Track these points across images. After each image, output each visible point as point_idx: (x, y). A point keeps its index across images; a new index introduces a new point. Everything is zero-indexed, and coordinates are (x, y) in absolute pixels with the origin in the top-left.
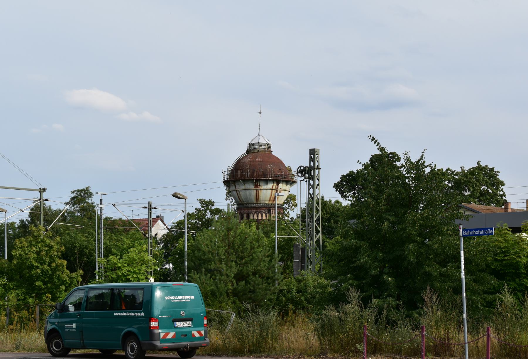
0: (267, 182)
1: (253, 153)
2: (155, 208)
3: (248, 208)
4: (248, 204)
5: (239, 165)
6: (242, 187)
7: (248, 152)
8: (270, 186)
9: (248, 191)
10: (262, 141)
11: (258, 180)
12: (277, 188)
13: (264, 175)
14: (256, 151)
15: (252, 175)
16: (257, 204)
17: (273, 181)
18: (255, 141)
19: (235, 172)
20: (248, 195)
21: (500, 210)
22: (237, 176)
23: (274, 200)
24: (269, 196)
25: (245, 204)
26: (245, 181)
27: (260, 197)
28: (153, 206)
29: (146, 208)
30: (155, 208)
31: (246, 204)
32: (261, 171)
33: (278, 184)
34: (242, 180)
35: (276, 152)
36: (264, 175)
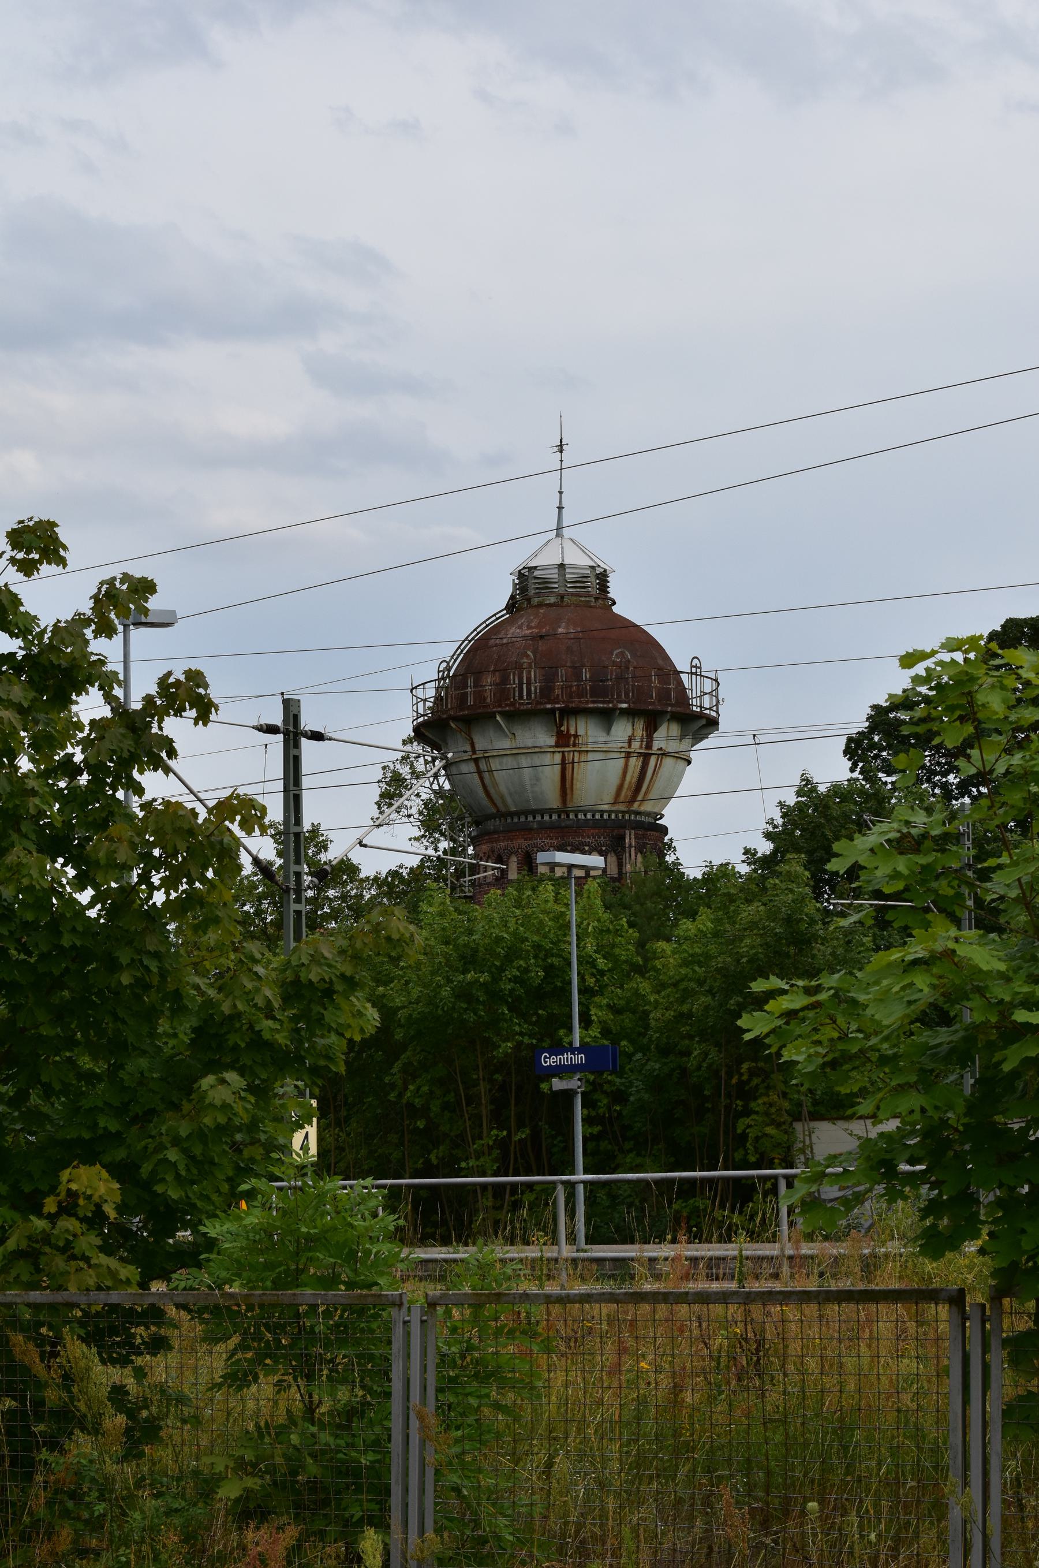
0: (607, 717)
1: (540, 605)
2: (317, 736)
3: (526, 830)
4: (526, 813)
5: (482, 654)
6: (504, 744)
7: (512, 606)
8: (622, 730)
9: (525, 762)
10: (576, 559)
11: (571, 712)
12: (649, 746)
13: (599, 690)
14: (552, 600)
15: (546, 692)
16: (563, 811)
17: (631, 714)
18: (549, 559)
19: (470, 682)
20: (527, 782)
21: (107, 1159)
22: (479, 696)
23: (633, 800)
24: (614, 780)
25: (512, 814)
26: (518, 716)
27: (577, 785)
28: (308, 722)
29: (271, 729)
30: (317, 736)
31: (518, 814)
32: (586, 674)
33: (651, 728)
34: (501, 713)
35: (629, 603)
36: (599, 690)
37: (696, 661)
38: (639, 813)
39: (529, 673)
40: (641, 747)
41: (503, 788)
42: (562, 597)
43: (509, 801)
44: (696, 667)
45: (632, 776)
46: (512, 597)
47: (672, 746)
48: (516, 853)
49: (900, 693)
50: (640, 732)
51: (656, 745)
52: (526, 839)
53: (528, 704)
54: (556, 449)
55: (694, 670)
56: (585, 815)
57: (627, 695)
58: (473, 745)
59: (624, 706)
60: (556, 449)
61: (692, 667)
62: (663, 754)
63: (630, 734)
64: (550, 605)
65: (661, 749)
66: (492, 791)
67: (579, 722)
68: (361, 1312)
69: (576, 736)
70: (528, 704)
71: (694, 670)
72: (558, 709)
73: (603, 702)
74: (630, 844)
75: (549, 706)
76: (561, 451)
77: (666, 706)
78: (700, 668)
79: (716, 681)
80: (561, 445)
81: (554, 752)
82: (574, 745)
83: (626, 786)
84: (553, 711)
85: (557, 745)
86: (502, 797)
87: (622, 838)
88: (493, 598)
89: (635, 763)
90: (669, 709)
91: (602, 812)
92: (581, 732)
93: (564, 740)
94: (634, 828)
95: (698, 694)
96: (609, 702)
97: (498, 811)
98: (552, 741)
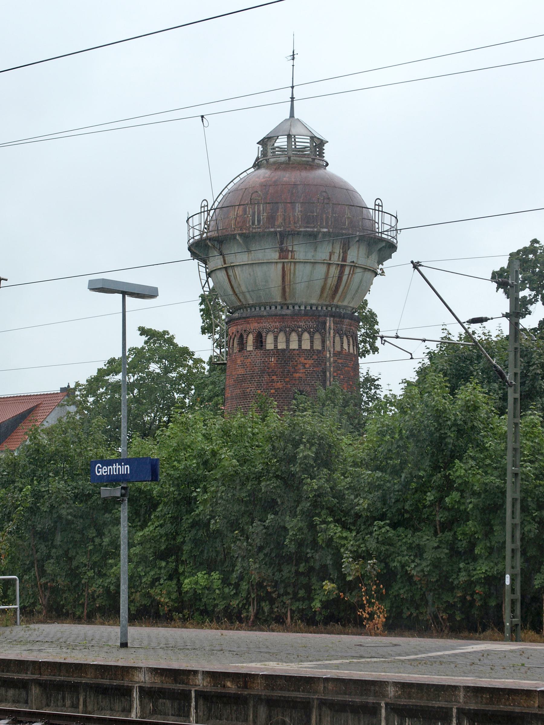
12: (344, 260)
31: (253, 306)
33: (345, 248)
37: (378, 202)
38: (337, 307)
44: (379, 205)
45: (331, 281)
46: (258, 159)
47: (362, 261)
50: (338, 250)
51: (349, 259)
53: (258, 228)
55: (377, 208)
56: (300, 307)
57: (327, 223)
59: (325, 230)
61: (375, 205)
62: (354, 266)
63: (330, 251)
65: (353, 262)
68: (319, 496)
71: (377, 208)
73: (311, 227)
74: (330, 328)
75: (272, 230)
76: (293, 59)
77: (367, 242)
78: (382, 206)
79: (396, 218)
80: (293, 55)
81: (277, 262)
83: (328, 286)
84: (275, 233)
87: (325, 323)
89: (334, 271)
90: (358, 233)
91: (311, 306)
93: (283, 252)
94: (334, 317)
95: (383, 225)
96: (314, 227)
98: (277, 255)
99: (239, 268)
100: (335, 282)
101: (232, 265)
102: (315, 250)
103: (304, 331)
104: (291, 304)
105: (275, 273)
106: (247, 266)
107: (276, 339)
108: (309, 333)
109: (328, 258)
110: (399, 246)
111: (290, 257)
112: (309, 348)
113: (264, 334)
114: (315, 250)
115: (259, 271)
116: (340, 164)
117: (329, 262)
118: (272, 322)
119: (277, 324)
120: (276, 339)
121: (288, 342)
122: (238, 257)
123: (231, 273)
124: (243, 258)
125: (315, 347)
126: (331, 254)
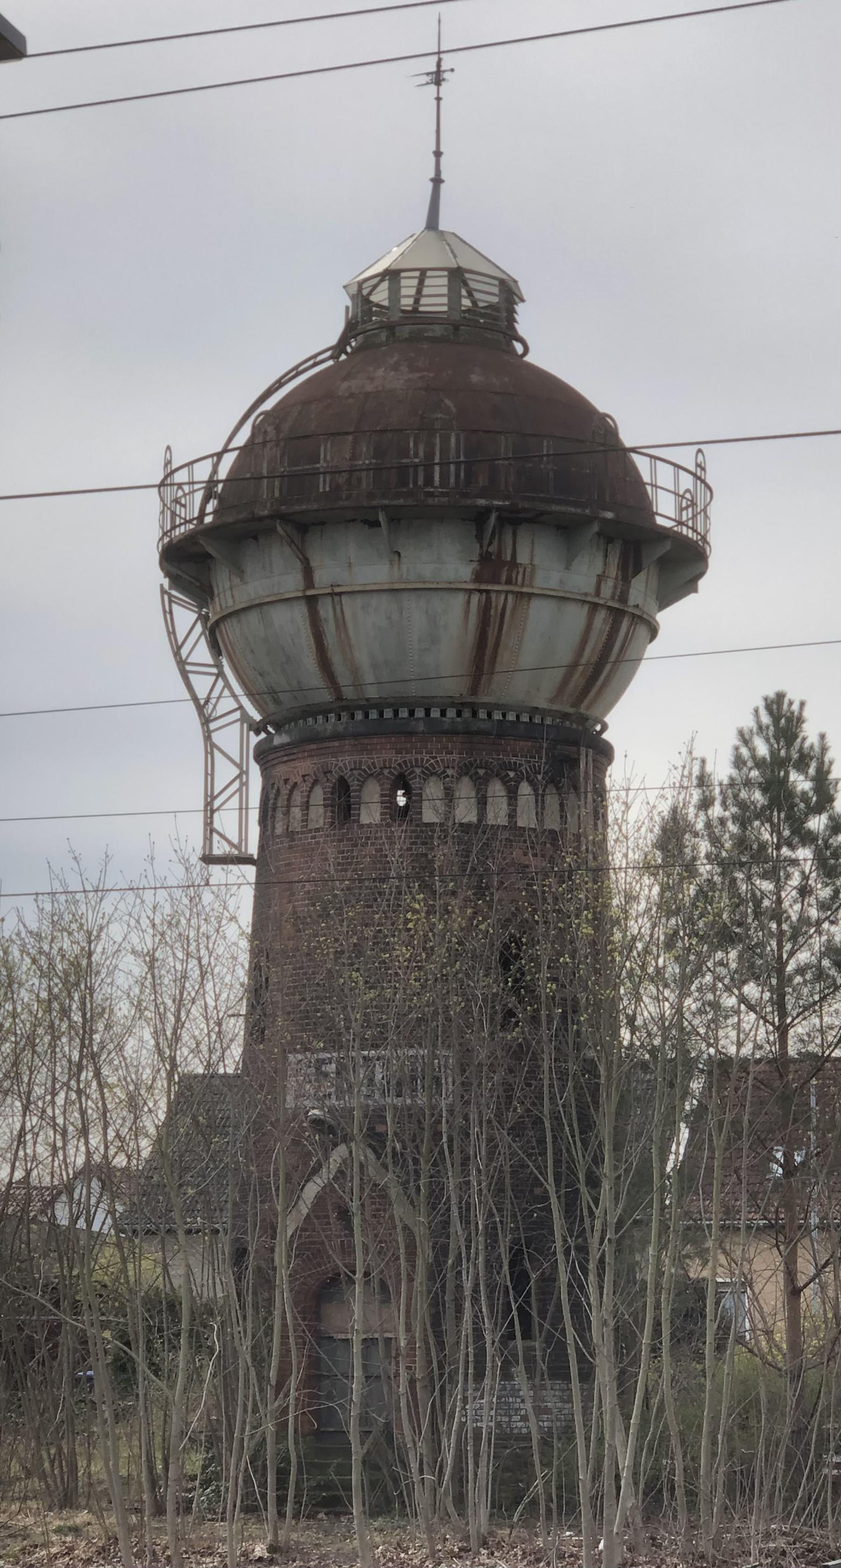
11: (513, 520)
39: (445, 440)
40: (612, 598)
41: (362, 658)
42: (456, 328)
43: (369, 677)
48: (378, 776)
49: (607, 719)
52: (399, 752)
53: (443, 495)
54: (427, 79)
58: (308, 573)
59: (609, 515)
60: (427, 79)
63: (599, 572)
64: (433, 340)
66: (336, 659)
67: (519, 540)
69: (513, 564)
70: (443, 495)
72: (499, 509)
82: (509, 582)
83: (584, 660)
85: (478, 578)
86: (355, 671)
88: (319, 327)
92: (523, 558)
93: (492, 568)
97: (339, 698)
99: (359, 600)
100: (595, 659)
101: (337, 590)
102: (567, 567)
103: (366, 779)
104: (484, 705)
105: (455, 619)
106: (385, 597)
107: (449, 796)
108: (505, 781)
109: (591, 590)
110: (154, 577)
111: (504, 578)
112: (503, 821)
113: (354, 784)
114: (567, 567)
115: (416, 611)
116: (551, 342)
117: (596, 600)
118: (439, 752)
119: (455, 756)
120: (449, 796)
121: (482, 802)
122: (351, 564)
123: (326, 610)
124: (375, 572)
125: (491, 820)
126: (601, 579)
